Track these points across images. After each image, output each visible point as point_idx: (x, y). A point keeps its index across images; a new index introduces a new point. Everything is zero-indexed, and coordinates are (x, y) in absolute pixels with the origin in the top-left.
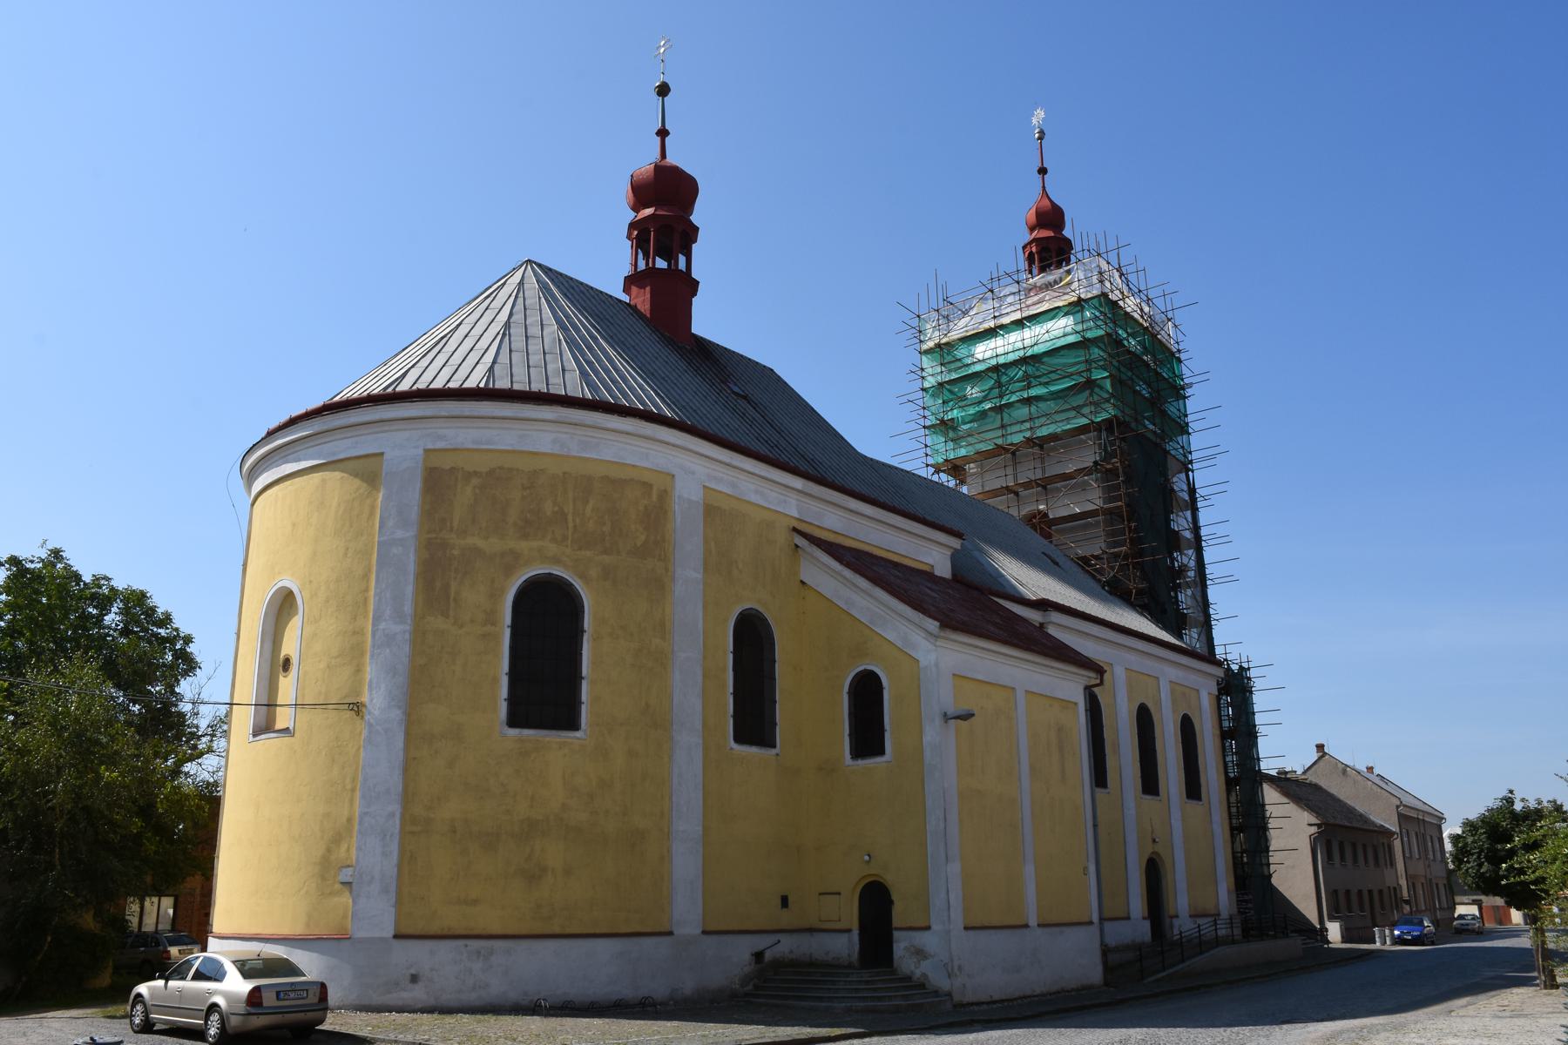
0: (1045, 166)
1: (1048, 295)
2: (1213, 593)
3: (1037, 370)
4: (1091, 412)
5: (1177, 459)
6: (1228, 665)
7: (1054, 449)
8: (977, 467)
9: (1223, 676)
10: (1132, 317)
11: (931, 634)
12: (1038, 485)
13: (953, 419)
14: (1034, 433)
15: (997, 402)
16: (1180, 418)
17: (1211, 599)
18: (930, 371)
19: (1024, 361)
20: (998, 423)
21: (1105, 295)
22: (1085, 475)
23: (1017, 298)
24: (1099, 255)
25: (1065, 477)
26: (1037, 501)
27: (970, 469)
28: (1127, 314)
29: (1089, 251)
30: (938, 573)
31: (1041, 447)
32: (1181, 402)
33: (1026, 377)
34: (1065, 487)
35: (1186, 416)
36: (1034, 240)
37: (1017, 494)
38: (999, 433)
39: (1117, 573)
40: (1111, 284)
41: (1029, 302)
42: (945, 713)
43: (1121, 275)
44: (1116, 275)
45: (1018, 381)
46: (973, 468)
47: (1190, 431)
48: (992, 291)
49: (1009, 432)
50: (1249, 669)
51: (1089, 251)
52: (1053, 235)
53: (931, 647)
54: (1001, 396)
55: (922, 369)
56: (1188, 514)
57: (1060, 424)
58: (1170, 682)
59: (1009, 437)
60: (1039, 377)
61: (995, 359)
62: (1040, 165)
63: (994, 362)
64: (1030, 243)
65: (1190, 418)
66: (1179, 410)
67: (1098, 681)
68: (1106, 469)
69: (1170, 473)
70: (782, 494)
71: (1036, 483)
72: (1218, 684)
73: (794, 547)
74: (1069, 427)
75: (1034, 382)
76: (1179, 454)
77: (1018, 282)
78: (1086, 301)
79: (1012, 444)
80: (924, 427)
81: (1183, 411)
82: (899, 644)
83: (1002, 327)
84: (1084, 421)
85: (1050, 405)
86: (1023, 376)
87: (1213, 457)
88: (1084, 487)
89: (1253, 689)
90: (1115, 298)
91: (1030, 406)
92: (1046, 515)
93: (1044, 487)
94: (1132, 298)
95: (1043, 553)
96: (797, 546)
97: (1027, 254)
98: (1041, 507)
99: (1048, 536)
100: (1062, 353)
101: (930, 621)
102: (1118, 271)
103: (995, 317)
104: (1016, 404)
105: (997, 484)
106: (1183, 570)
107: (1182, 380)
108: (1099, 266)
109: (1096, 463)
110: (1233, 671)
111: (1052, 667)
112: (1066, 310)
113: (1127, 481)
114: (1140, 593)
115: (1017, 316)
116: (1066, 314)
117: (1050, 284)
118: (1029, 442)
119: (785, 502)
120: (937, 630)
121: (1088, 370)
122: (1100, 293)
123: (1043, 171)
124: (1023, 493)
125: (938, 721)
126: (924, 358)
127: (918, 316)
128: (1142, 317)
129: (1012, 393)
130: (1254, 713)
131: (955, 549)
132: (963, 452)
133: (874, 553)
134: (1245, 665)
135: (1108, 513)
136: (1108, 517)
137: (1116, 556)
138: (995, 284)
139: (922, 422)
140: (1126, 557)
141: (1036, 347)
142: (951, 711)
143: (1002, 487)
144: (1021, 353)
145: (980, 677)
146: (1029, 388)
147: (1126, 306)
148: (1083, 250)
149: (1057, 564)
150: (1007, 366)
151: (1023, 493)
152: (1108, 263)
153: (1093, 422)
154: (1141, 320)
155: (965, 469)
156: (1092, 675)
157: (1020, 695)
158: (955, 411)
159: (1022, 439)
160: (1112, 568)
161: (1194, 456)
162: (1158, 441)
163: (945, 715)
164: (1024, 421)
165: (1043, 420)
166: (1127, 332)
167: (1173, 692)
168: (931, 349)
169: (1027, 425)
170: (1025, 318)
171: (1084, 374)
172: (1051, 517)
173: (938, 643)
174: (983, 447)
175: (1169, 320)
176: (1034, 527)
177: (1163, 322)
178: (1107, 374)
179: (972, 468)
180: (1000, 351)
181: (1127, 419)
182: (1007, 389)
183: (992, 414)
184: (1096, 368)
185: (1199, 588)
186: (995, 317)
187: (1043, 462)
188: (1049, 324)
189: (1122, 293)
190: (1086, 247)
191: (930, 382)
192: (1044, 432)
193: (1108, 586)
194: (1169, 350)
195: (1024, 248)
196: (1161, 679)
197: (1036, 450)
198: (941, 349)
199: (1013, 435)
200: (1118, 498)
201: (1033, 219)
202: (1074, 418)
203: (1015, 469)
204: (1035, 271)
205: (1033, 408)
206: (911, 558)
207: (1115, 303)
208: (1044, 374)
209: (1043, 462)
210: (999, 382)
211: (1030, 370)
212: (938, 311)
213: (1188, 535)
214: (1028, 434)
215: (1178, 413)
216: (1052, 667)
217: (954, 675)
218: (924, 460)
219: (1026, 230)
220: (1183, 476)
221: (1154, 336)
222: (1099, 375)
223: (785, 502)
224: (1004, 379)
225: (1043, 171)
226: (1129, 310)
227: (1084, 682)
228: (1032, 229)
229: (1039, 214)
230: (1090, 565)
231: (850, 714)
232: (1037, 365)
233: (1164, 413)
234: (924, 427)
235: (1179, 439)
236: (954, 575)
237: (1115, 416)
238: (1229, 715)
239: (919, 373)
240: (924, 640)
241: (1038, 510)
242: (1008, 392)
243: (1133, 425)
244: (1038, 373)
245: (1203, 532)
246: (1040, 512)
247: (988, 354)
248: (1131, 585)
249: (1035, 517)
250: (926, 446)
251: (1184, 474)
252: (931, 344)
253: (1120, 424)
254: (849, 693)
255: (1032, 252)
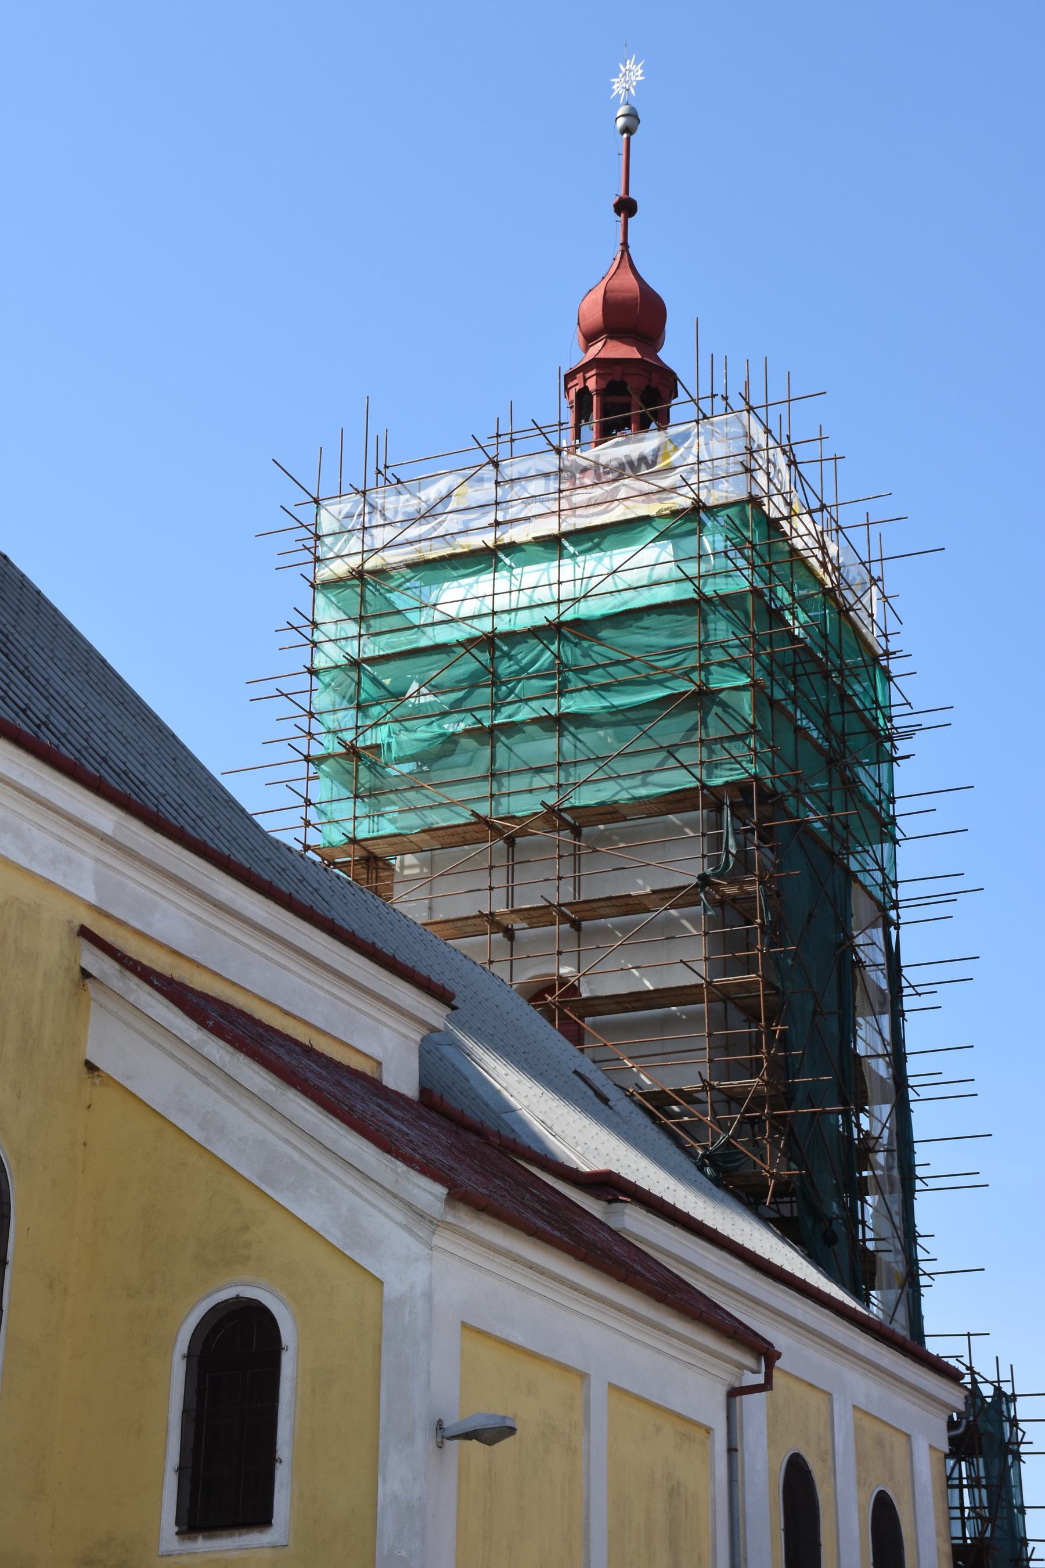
0: (631, 195)
1: (629, 486)
2: (923, 1206)
3: (585, 655)
4: (702, 763)
5: (870, 895)
6: (974, 1382)
7: (606, 839)
8: (421, 866)
9: (962, 1407)
10: (804, 561)
11: (421, 1215)
12: (565, 918)
13: (378, 746)
14: (566, 797)
15: (486, 718)
16: (879, 802)
17: (922, 1222)
18: (330, 630)
19: (555, 630)
20: (482, 767)
21: (754, 501)
22: (672, 907)
23: (553, 485)
24: (750, 409)
25: (629, 905)
26: (559, 953)
27: (403, 867)
28: (794, 551)
29: (725, 398)
30: (390, 1081)
31: (577, 832)
32: (884, 767)
33: (560, 668)
34: (624, 929)
35: (892, 800)
36: (596, 363)
37: (509, 933)
38: (484, 789)
39: (731, 1137)
40: (770, 480)
41: (580, 497)
42: (440, 1423)
43: (792, 463)
44: (782, 461)
45: (540, 676)
46: (411, 867)
47: (899, 835)
48: (496, 465)
49: (504, 790)
50: (1013, 1398)
51: (725, 398)
52: (639, 356)
53: (417, 1248)
54: (495, 707)
55: (315, 625)
56: (885, 1020)
57: (627, 783)
58: (855, 1407)
59: (504, 800)
60: (586, 670)
61: (489, 619)
62: (622, 193)
63: (485, 626)
64: (584, 368)
65: (900, 807)
66: (879, 785)
67: (760, 1379)
68: (723, 895)
69: (853, 922)
70: (62, 840)
71: (562, 914)
72: (952, 1425)
73: (77, 974)
74: (643, 792)
75: (575, 683)
76: (871, 880)
77: (559, 451)
78: (712, 511)
79: (511, 818)
80: (308, 759)
81: (886, 787)
82: (334, 1236)
83: (511, 548)
84: (681, 780)
85: (605, 739)
86: (552, 665)
87: (949, 898)
88: (670, 933)
89: (1023, 1448)
90: (774, 514)
91: (561, 735)
92: (574, 990)
93: (576, 925)
94: (806, 518)
95: (576, 1072)
96: (85, 974)
97: (572, 393)
98: (565, 970)
99: (576, 1037)
100: (647, 621)
101: (425, 1182)
102: (784, 452)
103: (497, 523)
104: (528, 729)
105: (468, 907)
106: (867, 1146)
107: (890, 719)
108: (748, 435)
109: (703, 879)
110: (983, 1398)
111: (668, 1332)
112: (662, 525)
113: (775, 932)
114: (783, 1189)
115: (549, 527)
116: (662, 536)
117: (631, 463)
118: (553, 816)
119: (69, 860)
120: (440, 1206)
121: (703, 667)
122: (744, 496)
123: (626, 207)
124: (524, 932)
125: (423, 1440)
126: (320, 599)
127: (316, 501)
128: (823, 565)
129: (521, 701)
130: (1022, 1509)
131: (433, 1030)
132: (387, 828)
133: (256, 1016)
134: (1007, 1389)
135: (723, 996)
136: (719, 1006)
137: (732, 1098)
138: (504, 450)
139: (302, 744)
140: (758, 1101)
141: (583, 604)
142: (453, 1421)
143: (481, 915)
144: (552, 613)
145: (520, 1339)
146: (561, 694)
147: (794, 534)
148: (713, 396)
149: (605, 1101)
150: (513, 637)
151: (524, 932)
152: (768, 431)
153: (704, 786)
154: (820, 571)
155: (390, 868)
156: (748, 1361)
157: (598, 1390)
158: (384, 729)
159: (540, 809)
160: (723, 1126)
161: (903, 892)
162: (837, 848)
163: (440, 1426)
164: (539, 770)
165: (585, 771)
166: (792, 594)
167: (859, 1432)
168: (341, 579)
169: (551, 779)
170: (567, 535)
171: (695, 676)
172: (584, 995)
173: (436, 1241)
174: (439, 819)
175: (874, 581)
176: (548, 1014)
177: (864, 583)
178: (744, 680)
179: (408, 864)
180: (502, 603)
181: (781, 787)
182: (511, 691)
183: (467, 743)
184: (721, 664)
185: (898, 1195)
186: (497, 523)
187: (577, 866)
188: (618, 556)
189: (789, 504)
190: (719, 390)
191: (330, 655)
192: (586, 797)
193: (713, 1165)
194: (869, 648)
195: (569, 377)
196: (834, 1395)
197: (566, 836)
198: (364, 583)
199: (512, 798)
200: (748, 965)
201: (595, 314)
202: (661, 769)
203: (510, 876)
204: (589, 432)
205: (567, 743)
206: (334, 1038)
207: (772, 525)
208: (598, 666)
209: (577, 866)
210: (494, 674)
211: (569, 654)
212: (364, 493)
213: (882, 1068)
214: (552, 799)
215: (876, 792)
216: (668, 1332)
217: (464, 1325)
218: (300, 834)
219: (578, 339)
220: (878, 934)
221: (844, 612)
222: (724, 679)
223: (69, 860)
224: (505, 668)
225: (626, 207)
226: (798, 543)
227: (728, 1377)
228: (590, 338)
229: (612, 306)
230: (671, 1115)
231: (185, 1412)
232: (585, 644)
233: (851, 786)
234: (308, 759)
235: (877, 847)
236: (423, 1091)
237: (756, 777)
238: (962, 1508)
239: (307, 631)
240: (403, 1234)
241: (560, 977)
242: (512, 698)
243: (791, 803)
244: (586, 663)
245: (913, 1066)
246: (563, 980)
247: (469, 609)
248: (766, 1169)
249: (550, 989)
250: (308, 803)
251: (880, 930)
252: (339, 568)
253: (767, 796)
254: (189, 1357)
255: (586, 388)
